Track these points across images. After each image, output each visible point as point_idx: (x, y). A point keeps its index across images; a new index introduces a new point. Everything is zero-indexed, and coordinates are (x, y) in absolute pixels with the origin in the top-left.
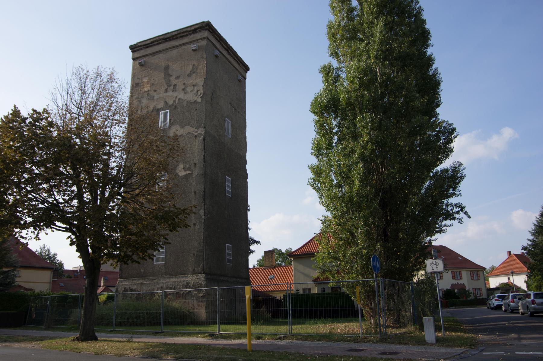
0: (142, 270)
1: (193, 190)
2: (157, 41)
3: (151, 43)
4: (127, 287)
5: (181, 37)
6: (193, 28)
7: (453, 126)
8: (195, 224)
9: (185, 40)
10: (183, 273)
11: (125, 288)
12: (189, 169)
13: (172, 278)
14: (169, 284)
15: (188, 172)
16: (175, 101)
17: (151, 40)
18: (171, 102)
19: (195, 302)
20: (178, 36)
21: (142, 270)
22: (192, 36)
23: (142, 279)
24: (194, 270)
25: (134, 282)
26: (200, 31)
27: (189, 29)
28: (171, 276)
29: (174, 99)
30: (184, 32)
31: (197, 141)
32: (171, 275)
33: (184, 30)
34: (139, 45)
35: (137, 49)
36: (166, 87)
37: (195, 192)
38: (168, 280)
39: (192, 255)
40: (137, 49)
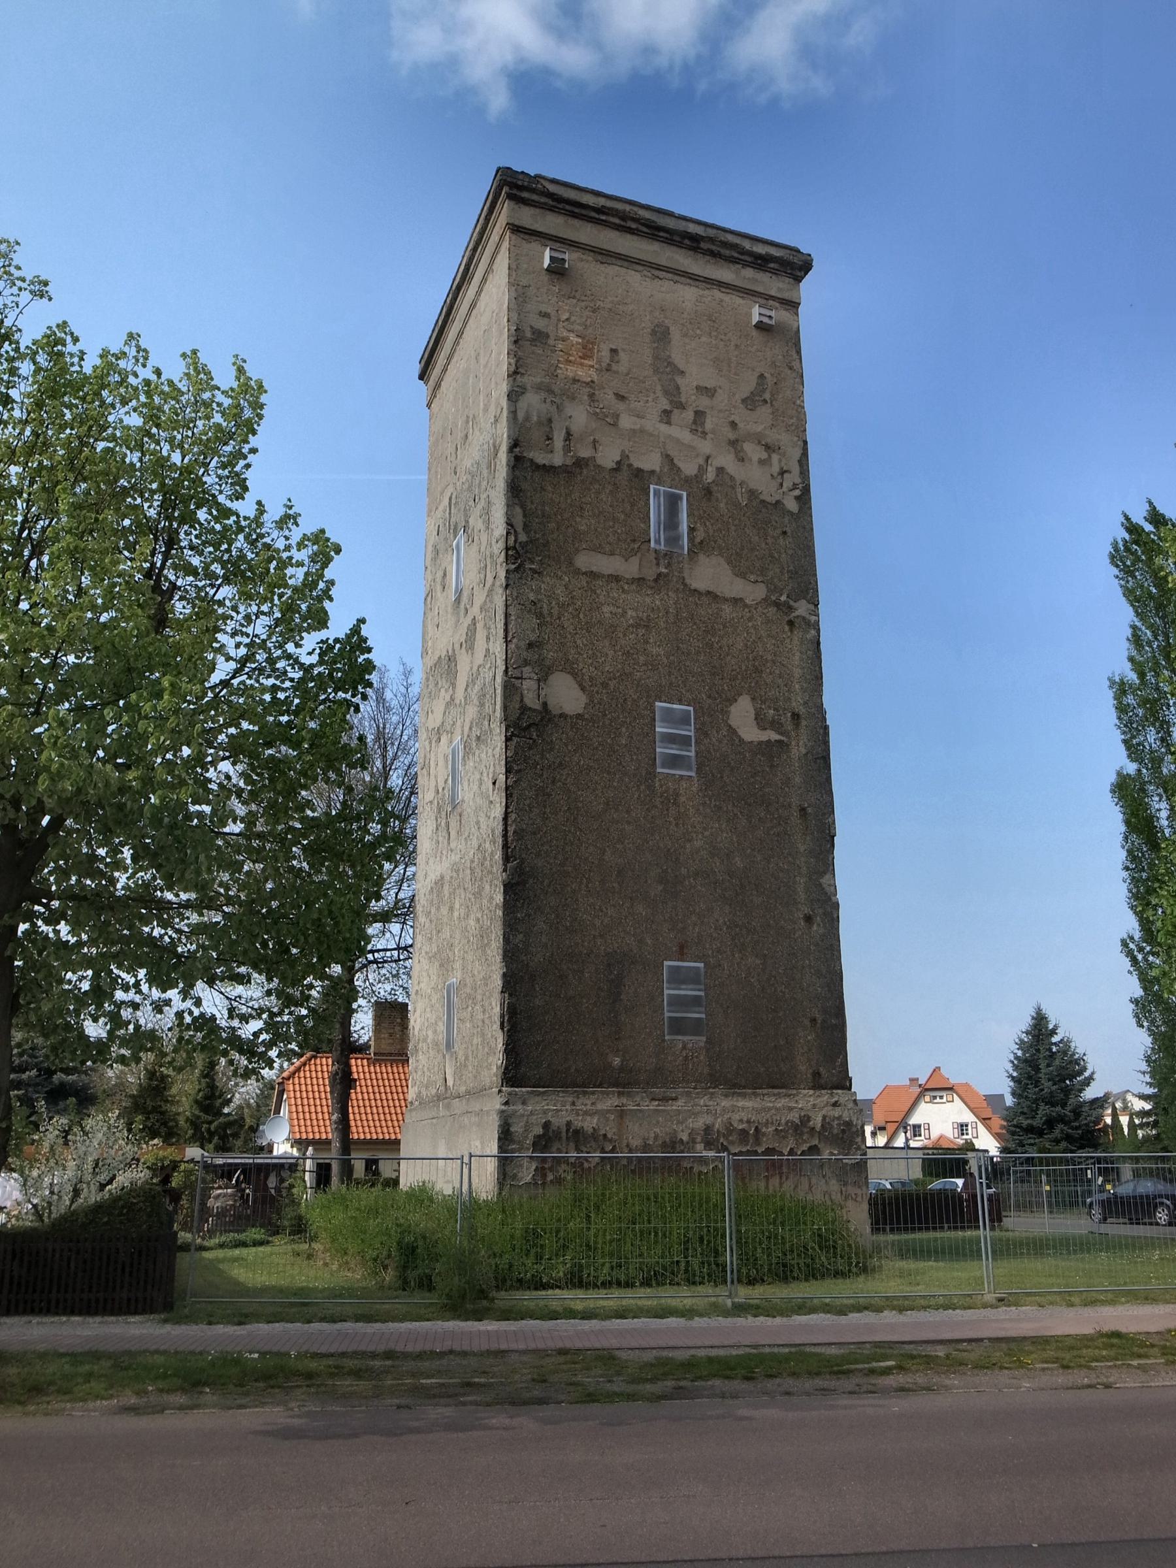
0: (617, 1061)
1: (795, 801)
2: (624, 216)
3: (600, 210)
4: (559, 1122)
5: (713, 254)
6: (760, 249)
7: (370, 656)
8: (808, 919)
9: (726, 274)
10: (780, 1082)
11: (547, 1125)
12: (775, 725)
13: (744, 1096)
14: (736, 1117)
15: (774, 736)
16: (702, 470)
17: (602, 202)
18: (689, 468)
19: (834, 1185)
20: (525, 195)
21: (617, 1061)
22: (749, 273)
23: (620, 1094)
24: (816, 1075)
25: (584, 1103)
26: (775, 272)
27: (747, 245)
28: (734, 1085)
29: (701, 461)
30: (725, 244)
31: (796, 641)
32: (735, 1086)
33: (731, 238)
34: (552, 188)
35: (535, 197)
36: (664, 404)
37: (803, 810)
38: (726, 1103)
39: (807, 1022)
40: (535, 197)
